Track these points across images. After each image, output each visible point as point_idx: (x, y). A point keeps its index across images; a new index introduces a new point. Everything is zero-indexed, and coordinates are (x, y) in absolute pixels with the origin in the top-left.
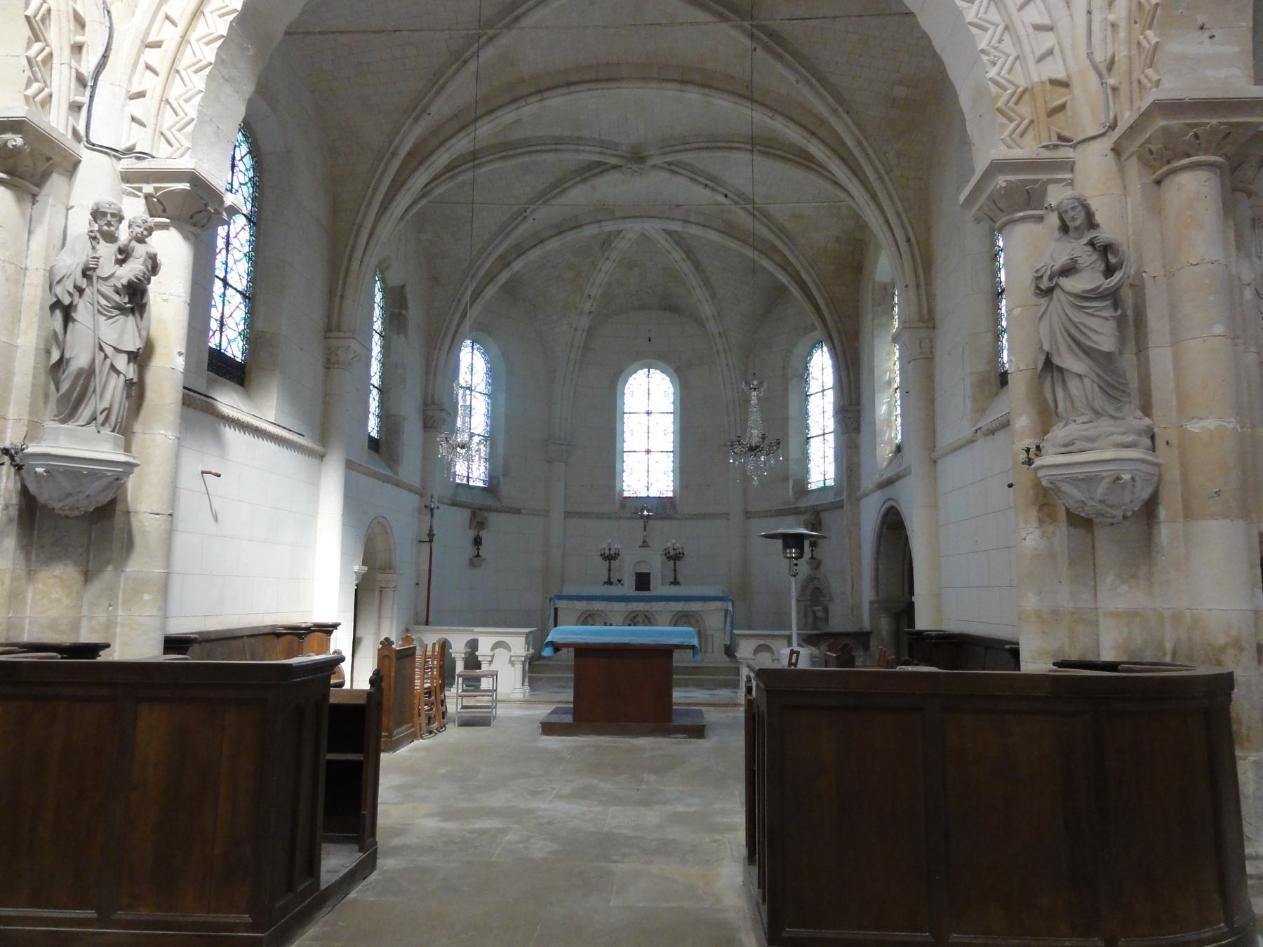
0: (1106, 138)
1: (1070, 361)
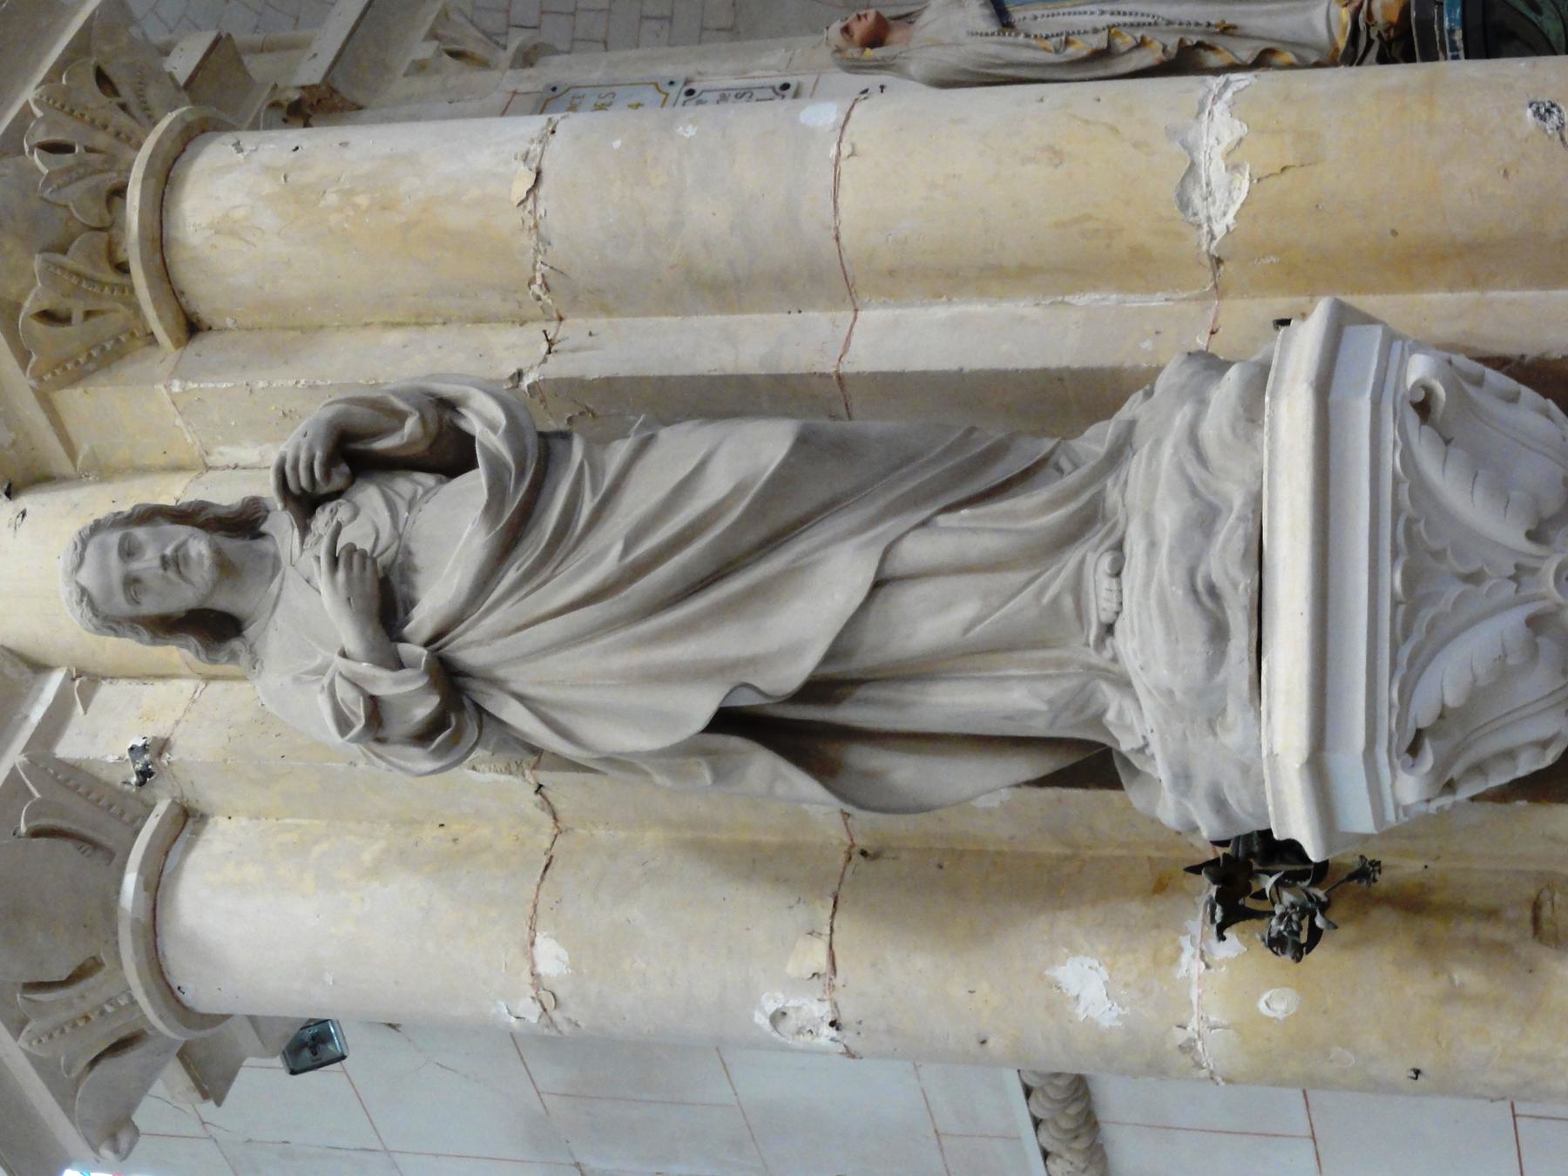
1: (791, 630)
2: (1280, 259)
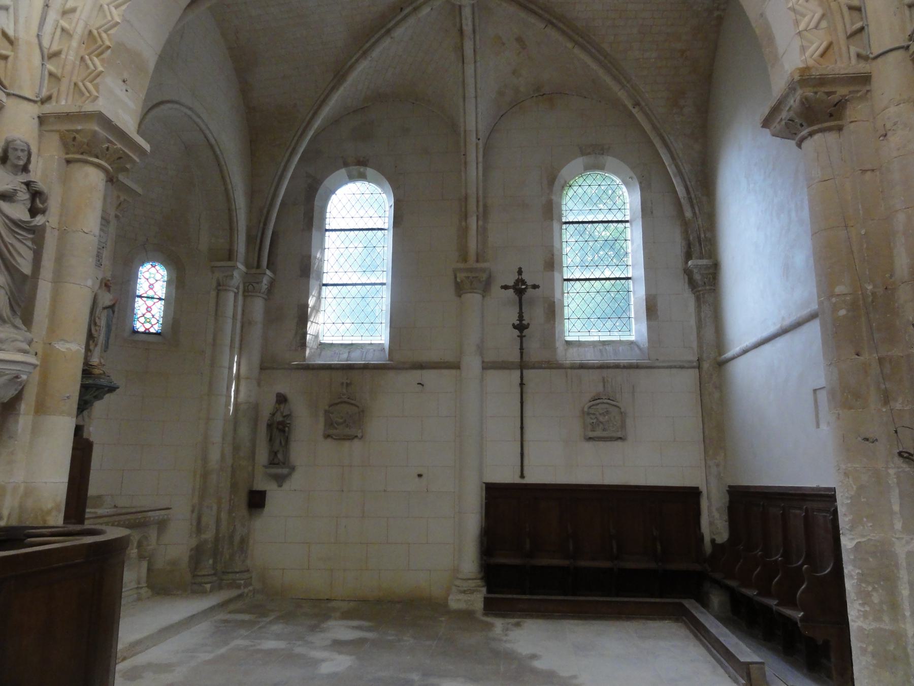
0: (36, 106)
2: (45, 369)
